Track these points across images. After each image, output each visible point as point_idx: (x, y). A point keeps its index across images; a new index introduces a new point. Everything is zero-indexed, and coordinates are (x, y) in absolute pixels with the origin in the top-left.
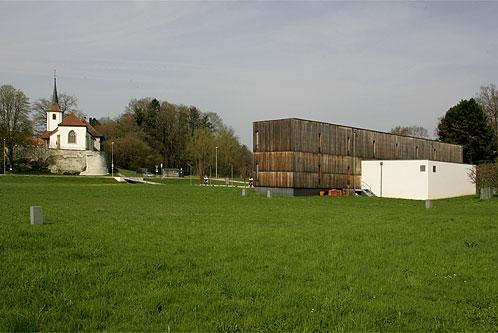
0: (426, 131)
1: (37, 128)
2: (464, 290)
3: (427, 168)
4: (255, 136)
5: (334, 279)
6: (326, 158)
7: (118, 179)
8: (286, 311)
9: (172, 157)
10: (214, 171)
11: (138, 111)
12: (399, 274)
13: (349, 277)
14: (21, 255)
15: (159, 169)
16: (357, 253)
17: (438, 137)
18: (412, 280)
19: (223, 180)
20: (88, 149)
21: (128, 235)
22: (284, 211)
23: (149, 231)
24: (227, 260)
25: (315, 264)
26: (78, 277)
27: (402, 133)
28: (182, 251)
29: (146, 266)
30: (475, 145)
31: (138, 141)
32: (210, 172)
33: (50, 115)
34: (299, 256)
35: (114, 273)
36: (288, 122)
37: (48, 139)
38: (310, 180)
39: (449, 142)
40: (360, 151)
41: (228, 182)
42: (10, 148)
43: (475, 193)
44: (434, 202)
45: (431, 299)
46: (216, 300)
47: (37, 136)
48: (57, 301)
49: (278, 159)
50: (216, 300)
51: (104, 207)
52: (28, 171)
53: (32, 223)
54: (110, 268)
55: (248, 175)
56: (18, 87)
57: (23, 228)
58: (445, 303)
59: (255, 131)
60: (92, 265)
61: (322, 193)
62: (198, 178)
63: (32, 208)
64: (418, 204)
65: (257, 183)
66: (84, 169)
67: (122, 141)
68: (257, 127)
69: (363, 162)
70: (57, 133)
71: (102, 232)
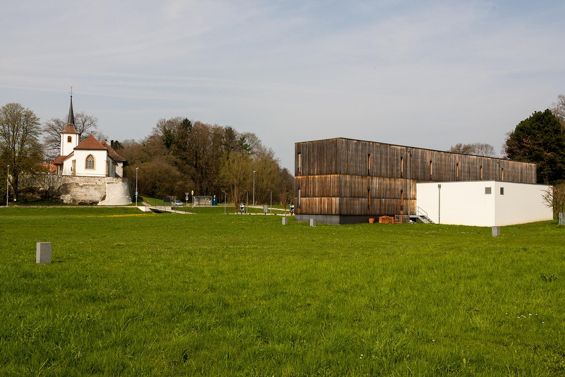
0: (492, 148)
1: (49, 152)
2: (543, 333)
3: (493, 191)
4: (297, 158)
5: (386, 319)
6: (376, 182)
7: (143, 209)
8: (330, 357)
9: (205, 184)
10: (250, 198)
11: (167, 133)
12: (462, 312)
13: (404, 317)
14: (22, 300)
15: (190, 196)
16: (412, 289)
17: (506, 155)
18: (477, 320)
19: (261, 207)
20: (108, 175)
21: (151, 272)
22: (329, 240)
23: (176, 267)
24: (264, 298)
25: (363, 301)
26: (90, 324)
27: (465, 151)
28: (212, 289)
29: (171, 308)
30: (552, 162)
31: (166, 166)
32: (247, 198)
33: (65, 137)
34: (346, 292)
35: (134, 317)
36: (334, 143)
37: (61, 165)
38: (358, 205)
39: (520, 160)
40: (415, 172)
41: (266, 210)
42: (15, 175)
43: (106, 152)
44: (503, 229)
45: (501, 342)
46: (250, 345)
47: (47, 161)
48: (62, 354)
49: (323, 183)
50: (250, 345)
51: (126, 241)
52: (36, 202)
53: (38, 261)
54: (129, 311)
55: (288, 202)
56: (27, 105)
57: (26, 267)
58: (519, 348)
59: (298, 152)
60: (107, 308)
61: (371, 220)
62: (233, 205)
63: (38, 245)
64: (487, 230)
65: (298, 210)
66: (104, 198)
67: (149, 166)
68: (300, 148)
69: (418, 185)
70: (72, 158)
71: (122, 270)
